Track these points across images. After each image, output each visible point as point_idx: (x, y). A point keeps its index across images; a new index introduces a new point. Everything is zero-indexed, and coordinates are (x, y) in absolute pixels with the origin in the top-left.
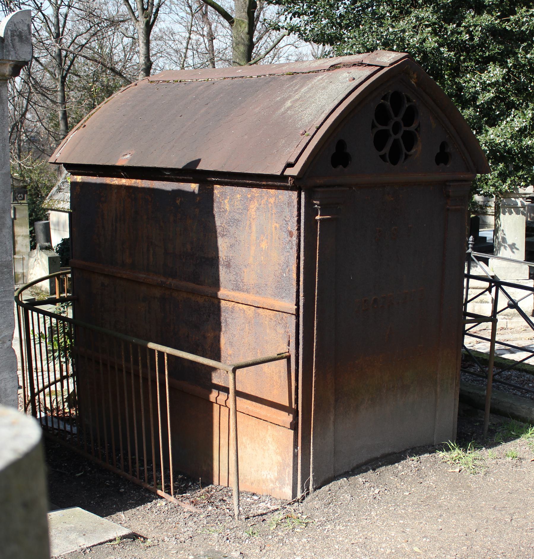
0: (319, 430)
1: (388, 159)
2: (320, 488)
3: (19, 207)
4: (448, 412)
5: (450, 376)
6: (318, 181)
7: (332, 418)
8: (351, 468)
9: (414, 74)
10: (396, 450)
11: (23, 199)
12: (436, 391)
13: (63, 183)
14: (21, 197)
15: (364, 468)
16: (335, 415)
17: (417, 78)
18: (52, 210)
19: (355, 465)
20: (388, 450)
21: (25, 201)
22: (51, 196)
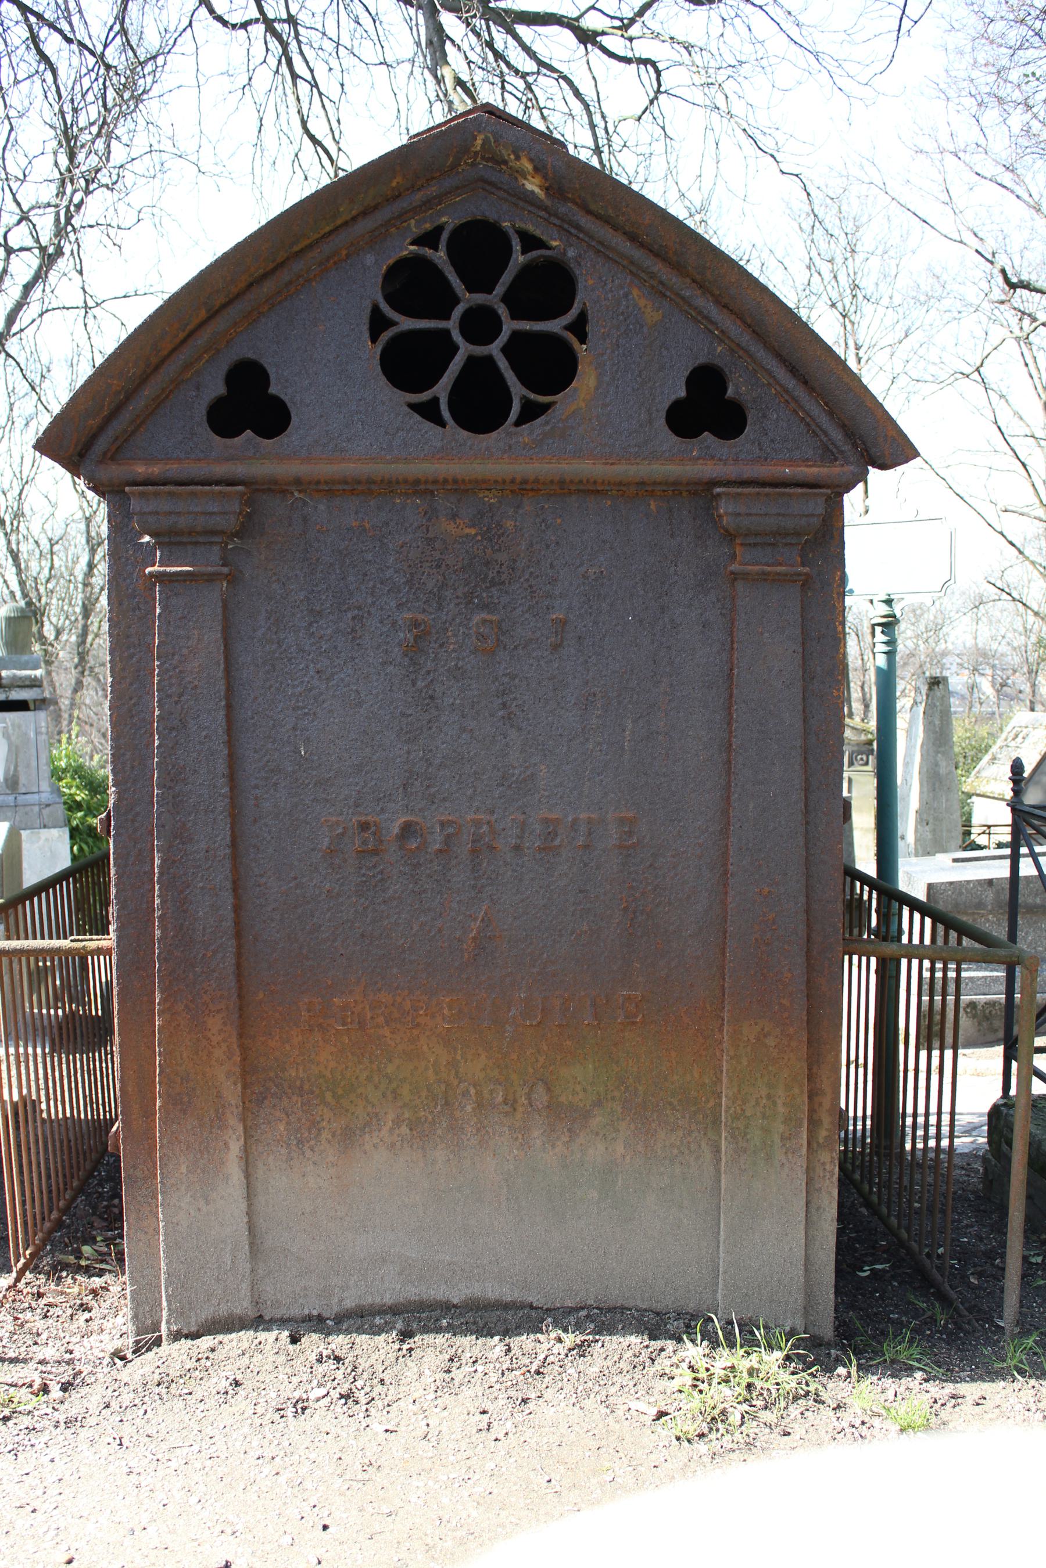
0: (183, 1169)
1: (446, 414)
2: (195, 1336)
3: (858, 777)
4: (784, 1229)
5: (781, 1109)
6: (217, 469)
7: (235, 1147)
8: (336, 1309)
9: (518, 158)
10: (531, 1298)
11: (867, 764)
12: (717, 1151)
13: (1001, 748)
14: (862, 759)
15: (378, 1321)
16: (248, 1135)
17: (536, 169)
18: (978, 795)
19: (349, 1304)
20: (492, 1291)
21: (869, 768)
22: (978, 772)
